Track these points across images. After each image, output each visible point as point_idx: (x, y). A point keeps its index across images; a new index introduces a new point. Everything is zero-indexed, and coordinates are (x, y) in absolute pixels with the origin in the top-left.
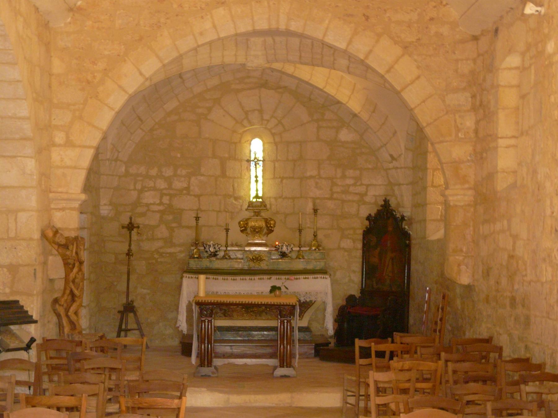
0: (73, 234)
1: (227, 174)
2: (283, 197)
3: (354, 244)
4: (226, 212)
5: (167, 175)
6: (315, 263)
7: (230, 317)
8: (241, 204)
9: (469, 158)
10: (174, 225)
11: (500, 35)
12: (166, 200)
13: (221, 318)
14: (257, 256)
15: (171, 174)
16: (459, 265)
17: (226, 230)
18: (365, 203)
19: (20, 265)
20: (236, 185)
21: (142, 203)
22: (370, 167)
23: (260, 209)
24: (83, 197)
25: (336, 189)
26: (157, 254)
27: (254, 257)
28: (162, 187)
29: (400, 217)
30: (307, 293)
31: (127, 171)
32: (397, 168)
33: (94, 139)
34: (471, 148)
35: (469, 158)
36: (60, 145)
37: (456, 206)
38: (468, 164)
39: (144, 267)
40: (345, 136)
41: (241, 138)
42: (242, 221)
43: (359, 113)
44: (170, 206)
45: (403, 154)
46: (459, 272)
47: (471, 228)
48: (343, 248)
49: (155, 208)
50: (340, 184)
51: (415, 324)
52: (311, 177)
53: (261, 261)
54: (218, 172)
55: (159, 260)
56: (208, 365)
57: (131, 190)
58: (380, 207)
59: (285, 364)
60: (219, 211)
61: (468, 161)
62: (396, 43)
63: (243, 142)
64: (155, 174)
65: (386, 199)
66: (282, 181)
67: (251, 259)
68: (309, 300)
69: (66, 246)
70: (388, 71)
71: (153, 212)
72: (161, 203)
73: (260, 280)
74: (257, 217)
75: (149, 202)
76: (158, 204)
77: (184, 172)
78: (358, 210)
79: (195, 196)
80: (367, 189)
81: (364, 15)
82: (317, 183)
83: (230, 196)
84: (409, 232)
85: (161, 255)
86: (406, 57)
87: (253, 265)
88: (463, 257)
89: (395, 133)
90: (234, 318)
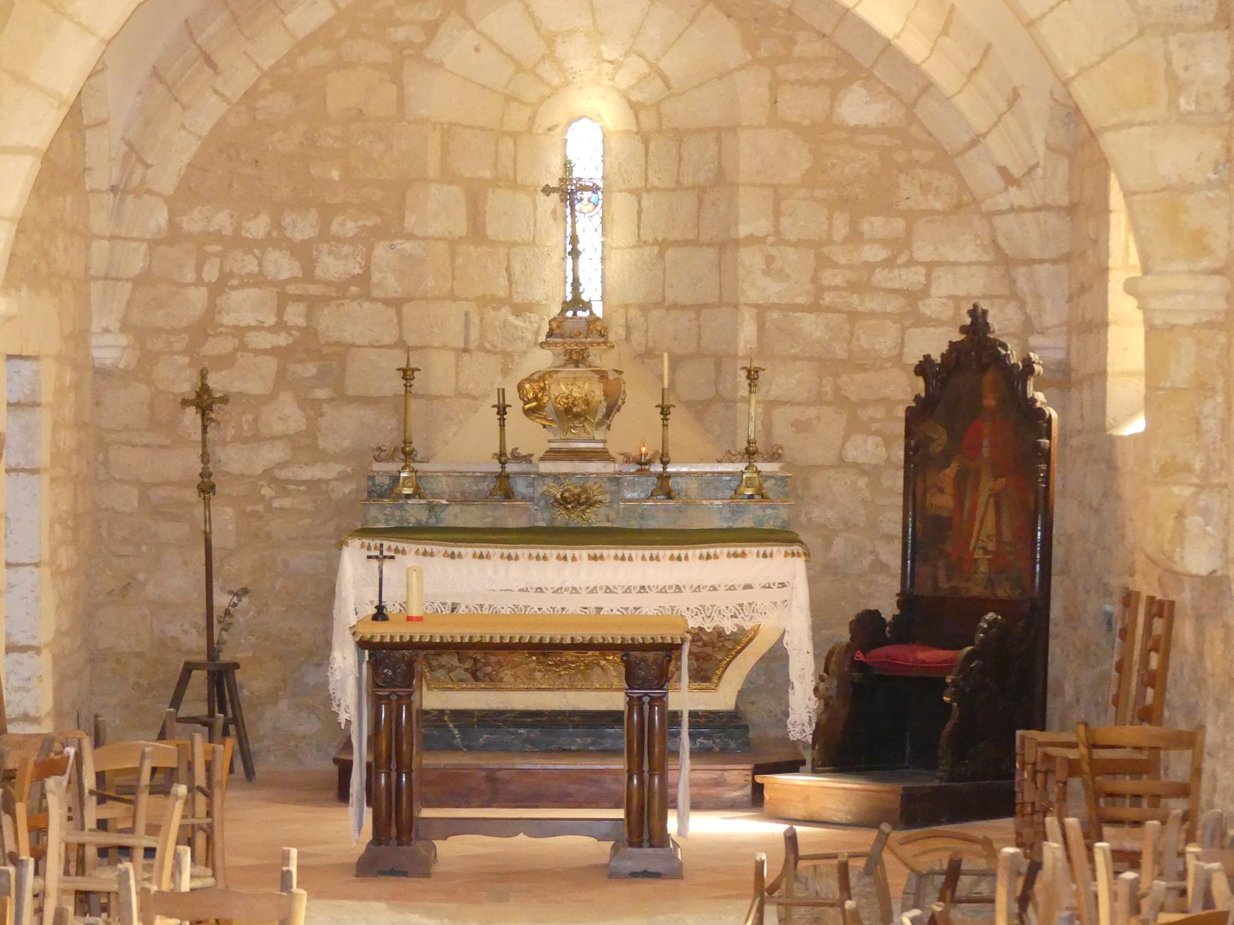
1: (490, 232)
2: (667, 303)
3: (888, 450)
4: (487, 351)
5: (298, 237)
6: (760, 513)
7: (491, 680)
8: (536, 325)
9: (1212, 176)
10: (322, 394)
12: (295, 315)
13: (464, 686)
14: (577, 491)
15: (312, 235)
16: (1181, 516)
17: (499, 409)
20: (517, 268)
21: (222, 325)
22: (938, 206)
23: (582, 343)
25: (831, 277)
26: (268, 486)
27: (567, 494)
28: (285, 275)
29: (1020, 364)
30: (741, 605)
31: (173, 224)
32: (1021, 210)
34: (1218, 144)
35: (1212, 176)
37: (1172, 327)
38: (1210, 194)
39: (230, 527)
41: (532, 119)
42: (529, 380)
43: (898, 36)
44: (309, 332)
45: (1042, 164)
46: (1180, 536)
47: (1220, 399)
48: (855, 465)
50: (842, 261)
51: (1078, 701)
52: (752, 240)
53: (591, 505)
54: (460, 228)
55: (276, 504)
56: (398, 838)
57: (188, 285)
58: (960, 335)
59: (646, 836)
60: (466, 350)
63: (540, 131)
64: (261, 235)
65: (975, 306)
66: (661, 255)
67: (556, 500)
68: (713, 625)
71: (258, 352)
72: (280, 326)
73: (676, 562)
74: (577, 367)
75: (243, 324)
77: (351, 228)
78: (902, 345)
79: (387, 302)
80: (928, 275)
82: (769, 260)
83: (498, 302)
84: (1047, 412)
85: (283, 487)
87: (561, 518)
88: (1192, 489)
89: (1014, 97)
90: (504, 686)
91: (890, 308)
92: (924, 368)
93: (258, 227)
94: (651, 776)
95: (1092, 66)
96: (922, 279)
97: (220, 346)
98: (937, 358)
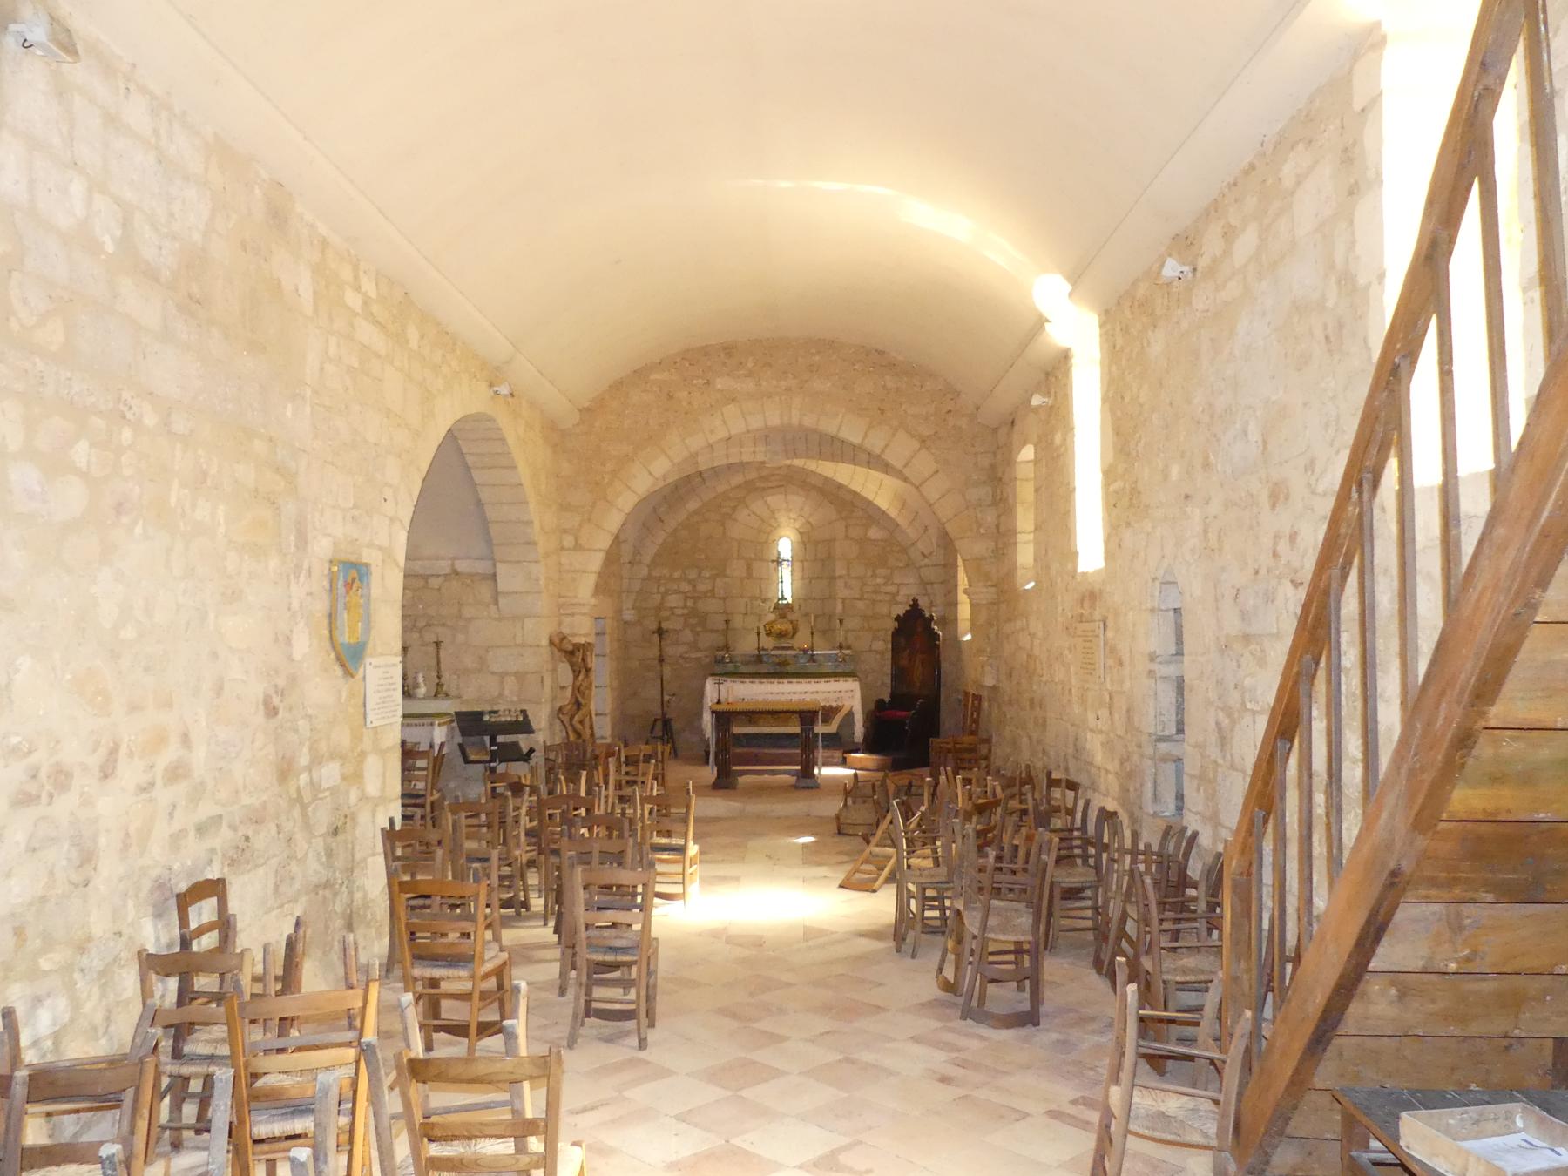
0: (582, 640)
11: (1016, 428)
12: (690, 603)
16: (983, 667)
18: (897, 603)
19: (527, 673)
24: (593, 601)
33: (604, 542)
36: (569, 549)
40: (874, 533)
49: (679, 612)
52: (840, 577)
61: (991, 557)
62: (913, 436)
69: (572, 653)
70: (906, 465)
72: (685, 607)
76: (683, 608)
81: (879, 409)
82: (846, 583)
83: (757, 598)
86: (924, 451)
87: (778, 669)
92: (898, 618)
97: (665, 613)
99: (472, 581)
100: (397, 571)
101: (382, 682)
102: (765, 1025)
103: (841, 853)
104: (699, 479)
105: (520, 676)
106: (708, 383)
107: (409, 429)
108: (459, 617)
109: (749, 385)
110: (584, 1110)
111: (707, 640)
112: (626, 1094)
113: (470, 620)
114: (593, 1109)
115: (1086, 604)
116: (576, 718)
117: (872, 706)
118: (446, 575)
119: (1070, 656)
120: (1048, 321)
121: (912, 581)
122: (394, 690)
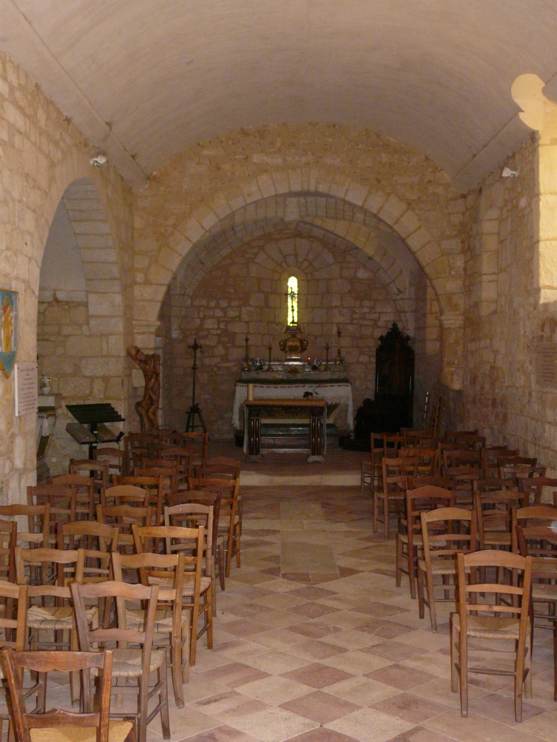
9: (460, 291)
10: (229, 345)
18: (379, 327)
20: (276, 313)
24: (158, 323)
28: (220, 315)
35: (460, 291)
36: (140, 284)
37: (450, 328)
40: (362, 274)
42: (282, 341)
43: (373, 256)
52: (335, 307)
55: (218, 372)
70: (396, 223)
72: (219, 328)
80: (379, 315)
82: (340, 312)
85: (219, 368)
91: (370, 324)
92: (381, 338)
93: (213, 304)
94: (318, 438)
95: (429, 264)
96: (378, 316)
97: (202, 333)
98: (384, 335)
99: (69, 307)
100: (34, 298)
101: (26, 382)
102: (328, 639)
103: (380, 559)
104: (232, 232)
105: (106, 379)
106: (247, 158)
107: (40, 190)
108: (58, 333)
109: (278, 160)
110: (209, 702)
111: (237, 353)
112: (238, 690)
113: (67, 336)
114: (216, 701)
115: (547, 329)
116: (151, 410)
117: (361, 404)
118: (49, 303)
119: (530, 368)
120: (522, 111)
121: (389, 310)
122: (33, 388)
